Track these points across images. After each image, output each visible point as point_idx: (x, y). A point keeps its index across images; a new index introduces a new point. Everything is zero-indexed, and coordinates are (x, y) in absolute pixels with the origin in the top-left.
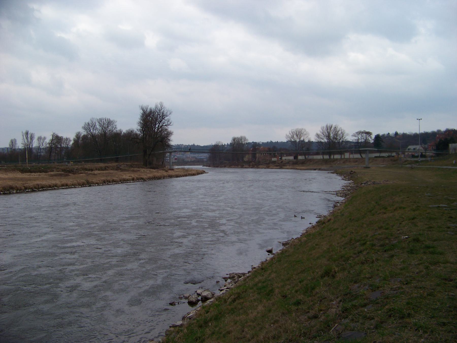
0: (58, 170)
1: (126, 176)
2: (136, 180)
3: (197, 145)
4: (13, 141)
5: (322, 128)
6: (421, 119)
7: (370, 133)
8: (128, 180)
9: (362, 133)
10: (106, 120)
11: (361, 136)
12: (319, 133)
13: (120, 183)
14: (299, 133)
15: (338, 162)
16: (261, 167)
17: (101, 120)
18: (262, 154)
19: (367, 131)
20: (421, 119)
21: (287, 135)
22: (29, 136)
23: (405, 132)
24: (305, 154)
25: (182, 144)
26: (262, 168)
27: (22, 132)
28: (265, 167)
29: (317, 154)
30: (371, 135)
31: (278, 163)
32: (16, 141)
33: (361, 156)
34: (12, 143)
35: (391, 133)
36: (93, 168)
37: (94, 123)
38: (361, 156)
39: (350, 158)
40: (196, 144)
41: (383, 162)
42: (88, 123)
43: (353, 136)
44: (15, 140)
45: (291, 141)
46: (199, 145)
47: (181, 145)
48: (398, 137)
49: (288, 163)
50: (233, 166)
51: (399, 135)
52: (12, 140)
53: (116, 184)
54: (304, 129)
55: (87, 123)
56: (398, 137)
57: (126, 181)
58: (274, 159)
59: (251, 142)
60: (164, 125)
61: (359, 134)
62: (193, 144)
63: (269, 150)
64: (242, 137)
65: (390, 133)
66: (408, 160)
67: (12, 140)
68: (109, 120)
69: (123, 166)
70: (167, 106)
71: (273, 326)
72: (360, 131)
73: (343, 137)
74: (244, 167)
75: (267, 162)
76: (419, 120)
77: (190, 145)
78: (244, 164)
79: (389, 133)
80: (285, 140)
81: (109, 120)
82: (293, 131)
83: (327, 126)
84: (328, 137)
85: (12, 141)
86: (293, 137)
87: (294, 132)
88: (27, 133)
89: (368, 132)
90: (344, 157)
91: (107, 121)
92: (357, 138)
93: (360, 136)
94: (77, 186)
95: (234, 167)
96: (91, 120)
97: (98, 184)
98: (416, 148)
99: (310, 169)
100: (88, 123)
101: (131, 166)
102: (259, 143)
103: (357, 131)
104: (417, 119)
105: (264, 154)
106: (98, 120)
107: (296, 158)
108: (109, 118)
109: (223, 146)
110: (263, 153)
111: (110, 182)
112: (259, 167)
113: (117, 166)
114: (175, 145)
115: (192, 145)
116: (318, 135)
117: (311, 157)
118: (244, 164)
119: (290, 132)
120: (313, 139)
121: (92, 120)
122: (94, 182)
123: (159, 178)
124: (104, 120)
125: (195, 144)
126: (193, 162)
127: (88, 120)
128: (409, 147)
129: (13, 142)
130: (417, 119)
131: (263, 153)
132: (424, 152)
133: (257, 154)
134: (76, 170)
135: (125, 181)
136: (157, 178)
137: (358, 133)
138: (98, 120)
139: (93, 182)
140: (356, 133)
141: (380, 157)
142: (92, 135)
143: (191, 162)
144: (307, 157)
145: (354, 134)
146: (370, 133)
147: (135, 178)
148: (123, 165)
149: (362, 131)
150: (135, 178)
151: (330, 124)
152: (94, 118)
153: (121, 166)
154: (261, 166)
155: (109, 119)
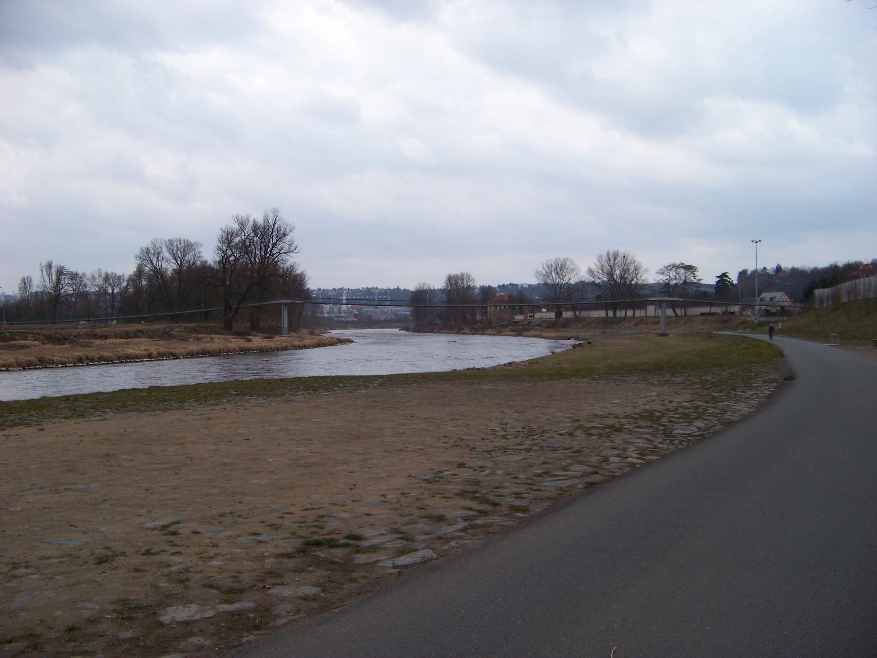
0: (37, 338)
1: (179, 347)
2: (155, 358)
3: (405, 290)
4: (26, 281)
5: (600, 258)
6: (760, 241)
7: (692, 269)
8: (137, 358)
9: (678, 267)
10: (180, 243)
11: (674, 273)
12: (593, 267)
13: (117, 363)
14: (560, 268)
15: (626, 325)
16: (489, 333)
17: (171, 242)
18: (498, 307)
19: (687, 263)
20: (760, 241)
21: (537, 272)
22: (54, 271)
23: (796, 266)
24: (574, 308)
25: (375, 287)
26: (490, 335)
27: (41, 264)
28: (495, 332)
29: (596, 308)
30: (696, 273)
31: (523, 325)
32: (31, 281)
33: (675, 313)
34: (25, 283)
35: (768, 268)
36: (108, 334)
37: (158, 247)
38: (675, 313)
39: (648, 317)
40: (402, 288)
41: (703, 324)
42: (148, 249)
43: (660, 273)
44: (31, 278)
45: (546, 284)
46: (408, 290)
47: (373, 288)
48: (781, 275)
49: (540, 325)
50: (446, 331)
51: (784, 271)
52: (24, 278)
53: (108, 364)
54: (570, 260)
55: (144, 249)
56: (781, 275)
57: (133, 358)
58: (519, 317)
59: (331, 288)
60: (282, 252)
61: (671, 269)
62: (396, 287)
63: (511, 298)
64: (462, 275)
65: (767, 268)
66: (748, 321)
67: (24, 278)
68: (186, 242)
69: (177, 330)
70: (287, 218)
71: (64, 643)
72: (673, 265)
73: (638, 276)
74: (434, 331)
75: (503, 323)
76: (757, 242)
77: (391, 288)
78: (464, 327)
79: (765, 268)
80: (534, 281)
81: (186, 242)
82: (549, 264)
83: (608, 254)
84: (611, 274)
85: (24, 281)
86: (548, 275)
87: (551, 265)
88: (50, 266)
89: (689, 266)
90: (646, 313)
91: (183, 244)
92: (668, 277)
93: (672, 274)
94: (13, 367)
95: (445, 333)
96: (153, 243)
97: (64, 365)
98: (775, 297)
99: (560, 337)
100: (148, 249)
101: (195, 331)
102: (522, 286)
103: (667, 264)
104: (753, 241)
105: (503, 307)
106: (165, 241)
107: (559, 314)
108: (186, 239)
109: (433, 291)
110: (490, 306)
111: (93, 360)
112: (486, 332)
113: (164, 329)
114: (363, 288)
115: (394, 289)
116: (591, 272)
117: (585, 314)
118: (464, 327)
119: (545, 266)
120: (586, 277)
121: (155, 242)
122: (56, 361)
123: (216, 353)
124: (178, 242)
125: (400, 287)
126: (389, 321)
127: (146, 243)
128: (763, 295)
129: (26, 283)
130: (753, 241)
131: (490, 306)
132: (793, 305)
133: (489, 307)
134: (74, 336)
135: (129, 359)
136: (209, 352)
137: (669, 268)
138: (165, 241)
139: (53, 360)
140: (665, 267)
141: (710, 314)
142: (156, 268)
143: (385, 321)
144: (577, 313)
145: (661, 270)
146: (694, 267)
147: (155, 353)
148: (177, 327)
149: (677, 263)
150: (155, 353)
151: (613, 250)
152: (158, 239)
153: (172, 329)
154: (489, 331)
155: (188, 241)
